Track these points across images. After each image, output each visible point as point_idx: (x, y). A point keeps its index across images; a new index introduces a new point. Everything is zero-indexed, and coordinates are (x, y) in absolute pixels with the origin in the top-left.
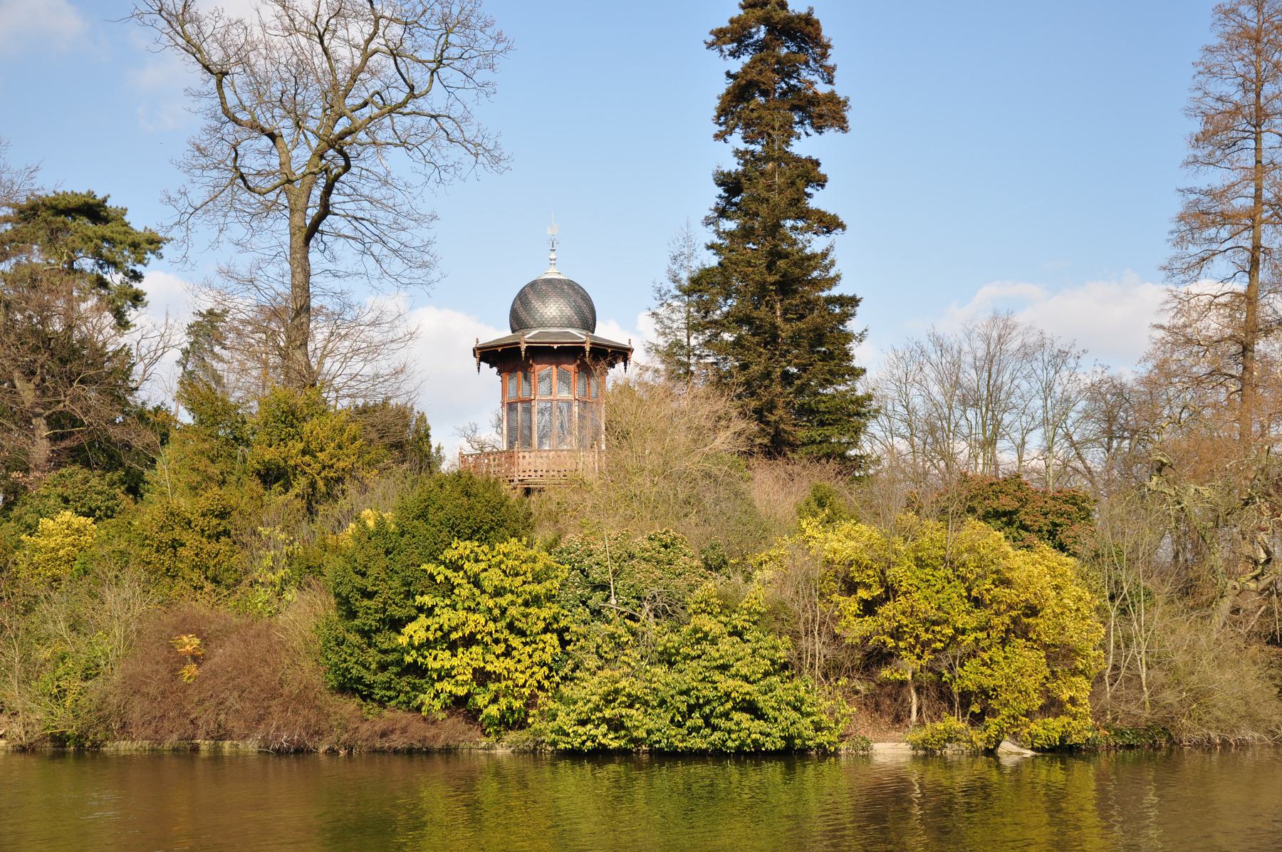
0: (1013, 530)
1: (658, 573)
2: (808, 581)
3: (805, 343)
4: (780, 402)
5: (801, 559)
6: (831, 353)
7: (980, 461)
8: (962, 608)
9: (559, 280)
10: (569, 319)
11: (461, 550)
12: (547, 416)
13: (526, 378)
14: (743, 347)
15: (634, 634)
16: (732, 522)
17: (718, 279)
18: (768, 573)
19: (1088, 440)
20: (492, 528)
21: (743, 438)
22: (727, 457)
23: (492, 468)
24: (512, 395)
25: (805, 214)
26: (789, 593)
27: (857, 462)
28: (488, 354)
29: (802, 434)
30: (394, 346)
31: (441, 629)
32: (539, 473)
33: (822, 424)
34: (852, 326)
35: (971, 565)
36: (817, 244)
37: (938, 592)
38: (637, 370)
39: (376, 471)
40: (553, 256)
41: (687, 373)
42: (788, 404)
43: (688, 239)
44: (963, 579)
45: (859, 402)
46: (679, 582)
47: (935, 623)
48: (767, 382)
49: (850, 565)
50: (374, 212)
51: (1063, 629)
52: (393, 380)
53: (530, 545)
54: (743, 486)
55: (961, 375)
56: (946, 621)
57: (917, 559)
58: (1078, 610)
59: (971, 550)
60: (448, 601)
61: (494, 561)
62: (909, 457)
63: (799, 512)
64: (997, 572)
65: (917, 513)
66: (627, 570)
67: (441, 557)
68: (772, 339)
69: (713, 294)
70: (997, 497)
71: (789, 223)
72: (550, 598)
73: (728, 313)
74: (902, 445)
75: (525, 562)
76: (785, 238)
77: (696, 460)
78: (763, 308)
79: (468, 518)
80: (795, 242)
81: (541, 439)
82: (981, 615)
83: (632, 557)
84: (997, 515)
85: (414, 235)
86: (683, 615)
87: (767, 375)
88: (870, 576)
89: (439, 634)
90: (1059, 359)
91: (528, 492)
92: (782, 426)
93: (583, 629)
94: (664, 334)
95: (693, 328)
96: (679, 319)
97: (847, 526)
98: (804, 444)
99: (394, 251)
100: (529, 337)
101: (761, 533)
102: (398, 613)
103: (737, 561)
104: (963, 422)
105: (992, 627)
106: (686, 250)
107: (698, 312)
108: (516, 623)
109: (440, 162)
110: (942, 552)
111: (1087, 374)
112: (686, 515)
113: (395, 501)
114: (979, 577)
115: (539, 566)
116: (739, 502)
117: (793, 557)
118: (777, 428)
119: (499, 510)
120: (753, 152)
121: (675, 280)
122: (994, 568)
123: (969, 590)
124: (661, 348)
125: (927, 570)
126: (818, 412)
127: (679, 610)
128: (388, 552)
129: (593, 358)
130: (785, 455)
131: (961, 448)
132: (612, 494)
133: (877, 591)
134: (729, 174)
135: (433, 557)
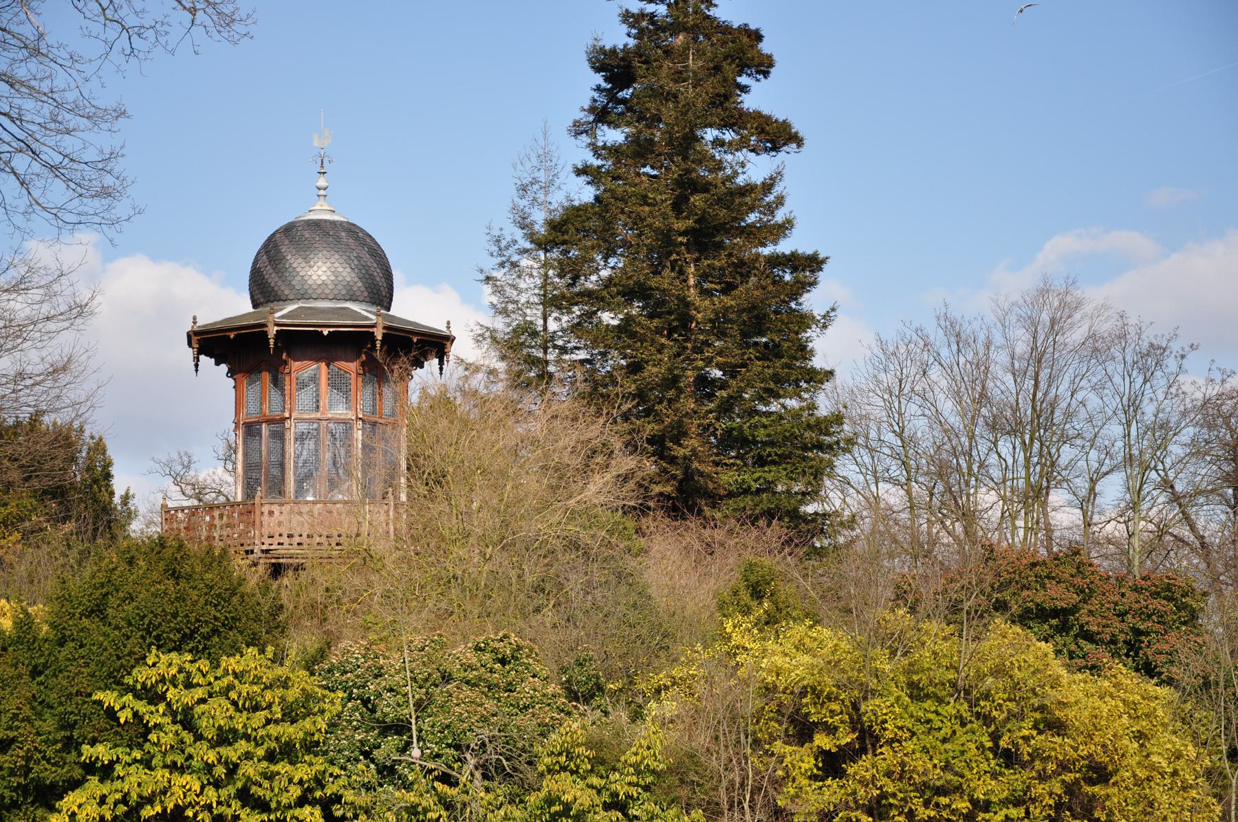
0: (1069, 640)
1: (490, 705)
2: (733, 720)
3: (734, 330)
4: (693, 427)
5: (723, 683)
6: (777, 346)
7: (1020, 523)
8: (984, 766)
9: (333, 223)
10: (348, 286)
11: (162, 669)
12: (310, 444)
13: (277, 382)
14: (633, 335)
15: (448, 806)
16: (613, 621)
17: (594, 223)
18: (670, 706)
19: (1199, 492)
20: (215, 631)
21: (631, 484)
22: (605, 516)
23: (221, 534)
24: (252, 409)
25: (738, 120)
26: (702, 739)
27: (817, 525)
28: (212, 343)
29: (728, 478)
30: (51, 326)
31: (124, 800)
32: (297, 539)
33: (761, 462)
34: (812, 302)
35: (999, 697)
36: (755, 168)
37: (944, 741)
38: (460, 371)
39: (17, 536)
40: (322, 182)
41: (540, 377)
42: (706, 428)
43: (545, 157)
44: (987, 719)
45: (823, 426)
46: (523, 720)
47: (941, 791)
48: (671, 393)
49: (803, 694)
50: (17, 102)
51: (1151, 805)
52: (49, 384)
53: (278, 659)
54: (631, 563)
55: (989, 384)
56: (958, 789)
57: (911, 685)
58: (1175, 773)
59: (998, 672)
60: (137, 754)
61: (217, 686)
62: (904, 516)
63: (722, 606)
64: (1042, 708)
65: (913, 610)
66: (440, 700)
67: (129, 680)
68: (678, 320)
69: (585, 249)
70: (1043, 586)
71: (710, 134)
72: (311, 746)
73: (610, 279)
74: (892, 496)
75: (269, 687)
76: (703, 159)
77: (555, 520)
78: (667, 272)
79: (175, 615)
80: (719, 166)
81: (300, 482)
82: (1016, 779)
83: (447, 678)
84: (1043, 614)
85: (87, 143)
86: (531, 776)
87: (672, 381)
88: (834, 714)
89: (122, 809)
90: (1151, 358)
91: (277, 570)
92: (695, 465)
93: (364, 799)
94: (504, 312)
95: (552, 302)
96: (529, 288)
97: (798, 630)
98: (731, 495)
99: (53, 168)
100: (282, 314)
101: (661, 642)
102: (48, 774)
103: (619, 685)
104: (993, 459)
105: (1033, 800)
106: (542, 176)
107: (561, 276)
108: (254, 789)
109: (131, 21)
110: (951, 675)
111: (1196, 384)
112: (537, 610)
113: (50, 586)
114: (1011, 716)
115: (293, 694)
116: (624, 589)
117: (709, 680)
118: (687, 468)
119: (228, 601)
120: (652, 15)
121: (524, 223)
122: (1035, 702)
123: (995, 737)
124: (500, 336)
125: (928, 704)
126: (755, 442)
127: (523, 766)
128: (35, 673)
129: (388, 353)
130: (700, 512)
131: (987, 498)
132: (416, 575)
133: (846, 738)
134: (613, 51)
135: (114, 681)
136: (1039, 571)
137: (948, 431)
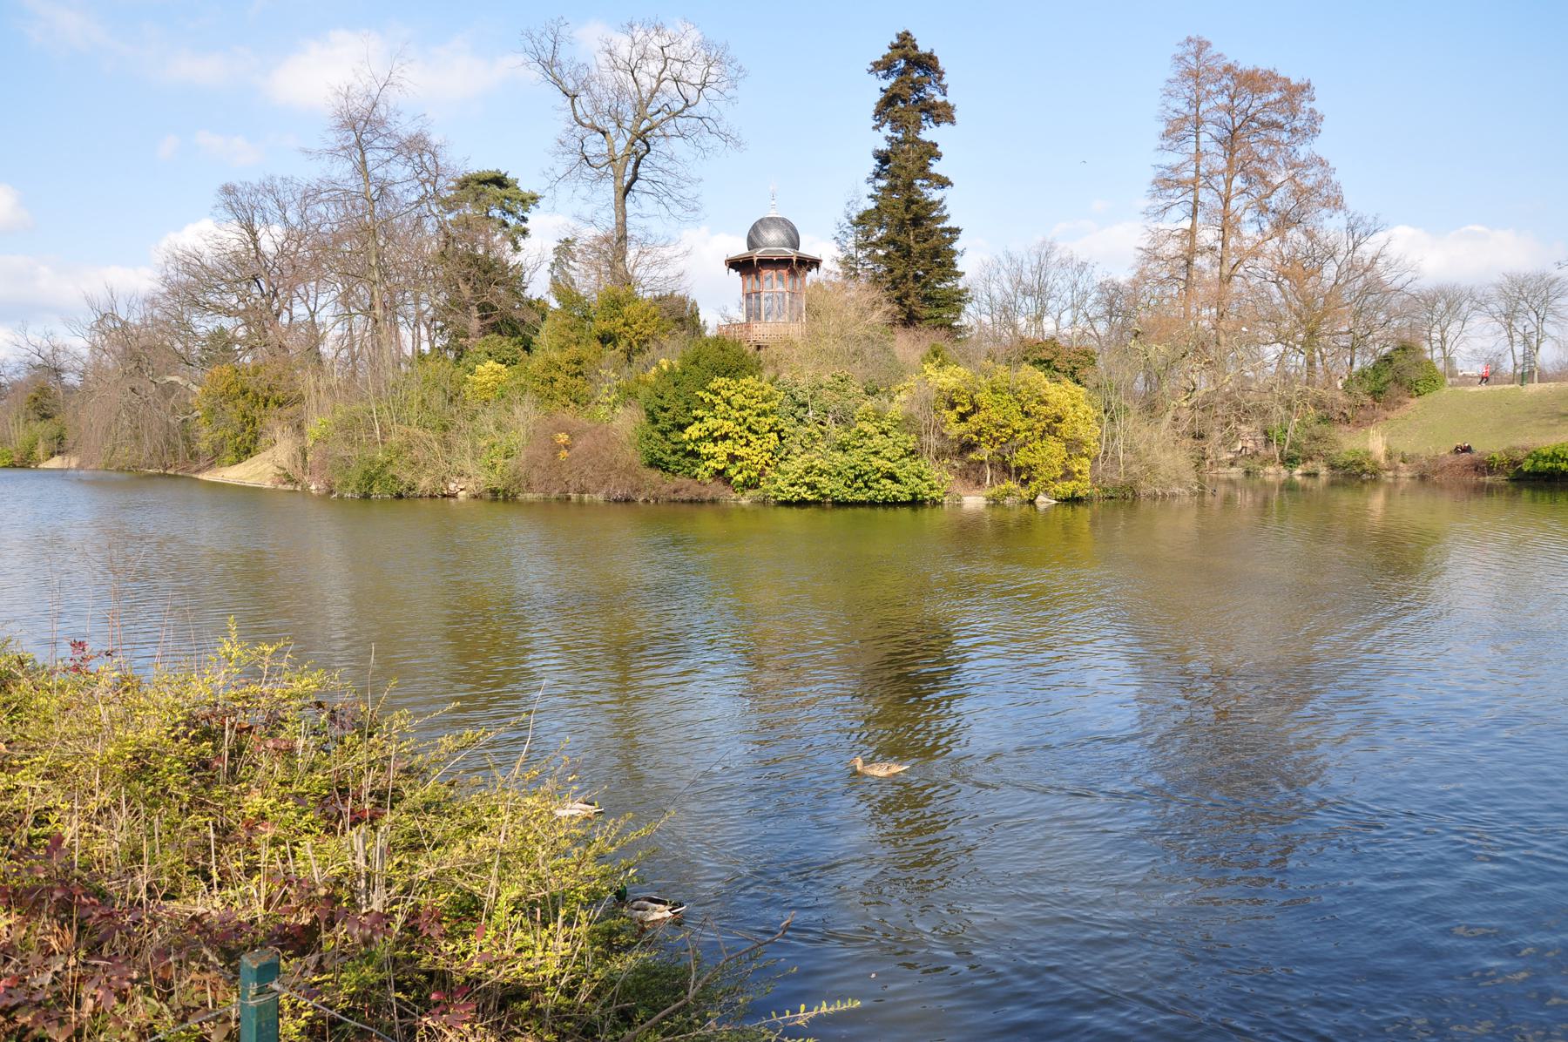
4: (912, 293)
18: (903, 397)
23: (739, 335)
24: (749, 288)
25: (928, 177)
26: (916, 409)
27: (959, 329)
28: (734, 264)
29: (925, 313)
33: (938, 306)
34: (956, 246)
45: (960, 293)
53: (760, 380)
54: (889, 344)
59: (1024, 383)
68: (907, 253)
71: (919, 182)
72: (773, 412)
74: (986, 319)
82: (1030, 421)
84: (1041, 362)
85: (689, 191)
87: (905, 276)
88: (964, 399)
90: (1082, 267)
95: (859, 247)
96: (851, 242)
100: (758, 254)
101: (900, 373)
102: (683, 421)
111: (1099, 276)
113: (679, 354)
115: (766, 393)
121: (849, 217)
131: (1022, 322)
133: (968, 408)
135: (703, 388)
136: (1039, 346)
137: (1007, 294)
